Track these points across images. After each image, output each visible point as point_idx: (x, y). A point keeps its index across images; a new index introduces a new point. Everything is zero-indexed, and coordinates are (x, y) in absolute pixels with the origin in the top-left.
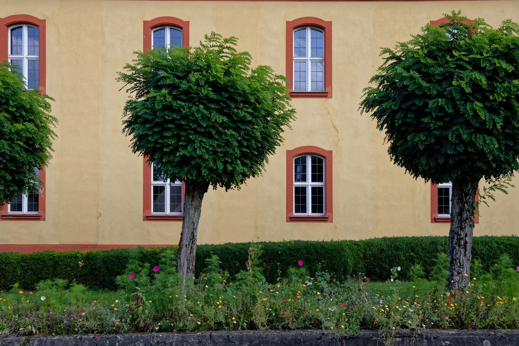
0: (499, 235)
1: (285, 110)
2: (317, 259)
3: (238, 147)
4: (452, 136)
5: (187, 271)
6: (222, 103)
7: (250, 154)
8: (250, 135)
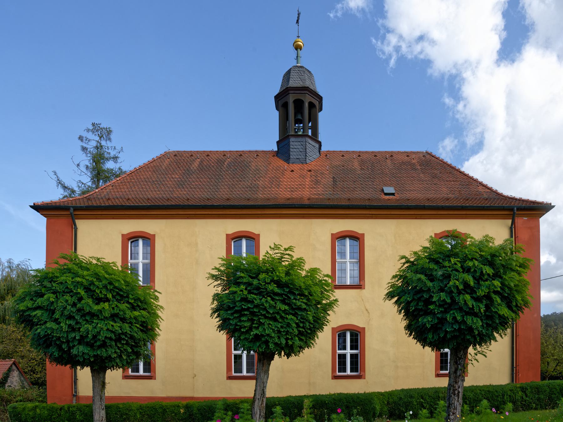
0: (482, 384)
1: (330, 300)
2: (354, 406)
3: (296, 328)
4: (450, 318)
5: (259, 417)
6: (284, 296)
7: (305, 332)
8: (305, 319)
